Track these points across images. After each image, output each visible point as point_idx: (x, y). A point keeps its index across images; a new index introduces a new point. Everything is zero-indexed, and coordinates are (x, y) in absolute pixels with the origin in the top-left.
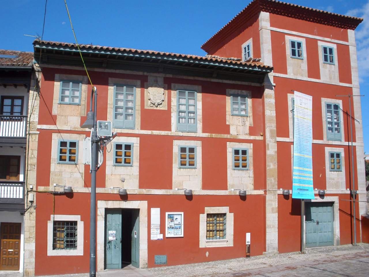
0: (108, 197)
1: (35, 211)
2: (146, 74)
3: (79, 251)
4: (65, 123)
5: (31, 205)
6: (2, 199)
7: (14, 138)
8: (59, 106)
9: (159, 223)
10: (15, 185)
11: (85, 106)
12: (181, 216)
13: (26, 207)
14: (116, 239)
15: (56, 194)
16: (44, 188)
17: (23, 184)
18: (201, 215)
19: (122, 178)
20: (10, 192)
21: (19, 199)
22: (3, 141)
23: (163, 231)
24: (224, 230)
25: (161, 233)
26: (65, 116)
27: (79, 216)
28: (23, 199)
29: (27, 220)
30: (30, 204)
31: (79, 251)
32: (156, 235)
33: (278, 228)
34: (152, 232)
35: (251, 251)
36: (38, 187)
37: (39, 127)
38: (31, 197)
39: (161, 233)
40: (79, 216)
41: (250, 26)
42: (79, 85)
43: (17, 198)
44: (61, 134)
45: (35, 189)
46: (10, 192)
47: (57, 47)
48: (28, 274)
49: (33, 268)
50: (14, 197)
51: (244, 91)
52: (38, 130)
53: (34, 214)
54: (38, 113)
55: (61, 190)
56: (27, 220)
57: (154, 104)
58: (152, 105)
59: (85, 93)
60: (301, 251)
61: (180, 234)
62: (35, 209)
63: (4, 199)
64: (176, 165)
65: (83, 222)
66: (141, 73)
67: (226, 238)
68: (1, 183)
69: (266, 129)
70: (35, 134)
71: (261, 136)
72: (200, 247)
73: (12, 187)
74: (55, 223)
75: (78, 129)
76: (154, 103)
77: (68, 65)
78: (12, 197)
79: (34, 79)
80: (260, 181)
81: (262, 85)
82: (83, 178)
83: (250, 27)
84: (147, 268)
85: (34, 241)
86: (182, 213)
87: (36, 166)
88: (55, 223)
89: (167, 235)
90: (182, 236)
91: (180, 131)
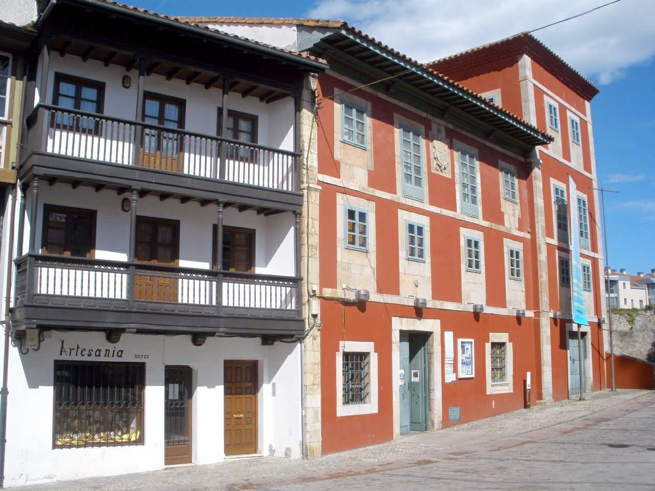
0: (402, 311)
1: (318, 333)
2: (430, 117)
3: (370, 407)
4: (351, 178)
5: (17, 308)
6: (84, 300)
7: (66, 158)
8: (341, 145)
9: (452, 356)
10: (119, 270)
11: (371, 152)
12: (471, 346)
13: (307, 328)
14: (405, 384)
15: (347, 303)
16: (332, 291)
17: (299, 281)
18: (486, 343)
19: (416, 280)
20: (115, 286)
21: (121, 300)
22: (265, 197)
23: (455, 370)
24: (501, 369)
25: (454, 372)
26: (350, 165)
27: (372, 344)
28: (299, 311)
29: (310, 351)
30: (312, 321)
31: (370, 407)
32: (451, 378)
33: (552, 366)
34: (446, 369)
35: (531, 401)
36: (323, 289)
37: (321, 177)
38: (315, 307)
39: (454, 372)
40: (372, 344)
41: (494, 71)
42: (352, 112)
43: (83, 295)
44: (347, 195)
45: (318, 293)
46: (68, 283)
47: (391, 57)
48: (313, 452)
49: (319, 441)
50: (91, 296)
51: (511, 166)
52: (320, 183)
53: (319, 339)
54: (316, 152)
55: (352, 297)
56: (310, 351)
57: (440, 167)
58: (438, 168)
59: (370, 130)
60: (568, 398)
61: (470, 373)
62: (319, 330)
63: (256, 310)
64: (464, 266)
65: (377, 353)
66: (424, 115)
67: (506, 380)
68: (194, 274)
69: (536, 224)
70: (316, 190)
71: (529, 233)
72: (487, 394)
73: (105, 274)
74: (347, 356)
75: (367, 191)
76: (441, 165)
77: (348, 75)
78: (80, 295)
79: (308, 89)
80: (533, 300)
81: (528, 160)
82: (374, 276)
83: (496, 73)
84: (442, 428)
85: (319, 390)
86: (472, 340)
87: (318, 249)
88: (347, 356)
89: (462, 375)
90: (473, 376)
91: (465, 214)
